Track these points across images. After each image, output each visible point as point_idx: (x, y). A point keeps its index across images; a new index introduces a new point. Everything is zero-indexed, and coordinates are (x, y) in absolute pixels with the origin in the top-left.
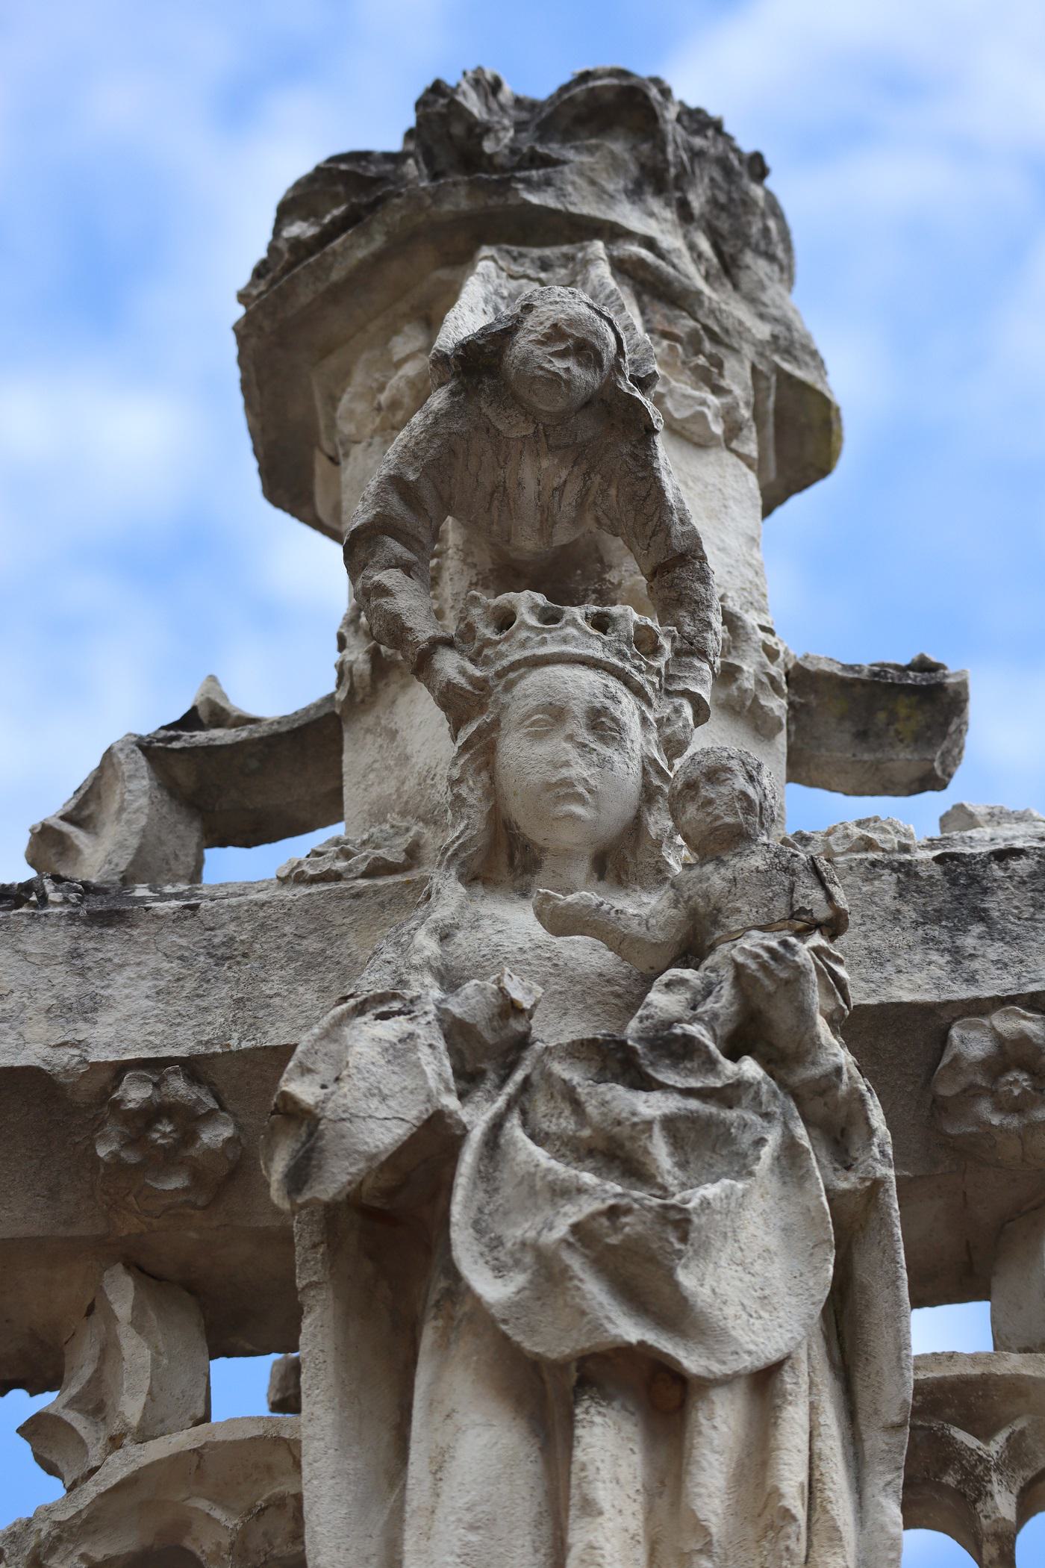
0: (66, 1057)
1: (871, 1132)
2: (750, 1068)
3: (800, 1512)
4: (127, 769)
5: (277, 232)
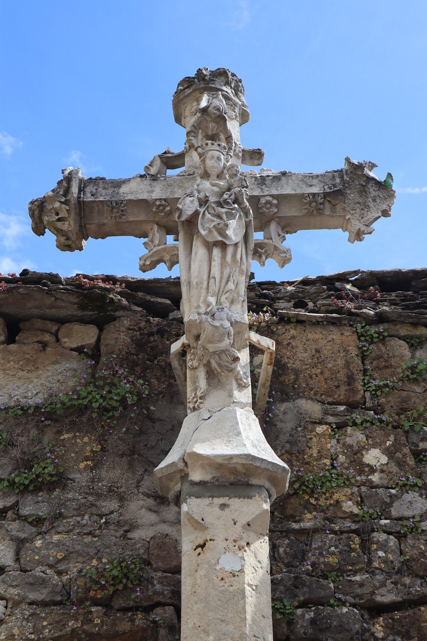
0: (149, 198)
1: (250, 213)
2: (236, 206)
3: (240, 261)
4: (157, 159)
5: (178, 87)
